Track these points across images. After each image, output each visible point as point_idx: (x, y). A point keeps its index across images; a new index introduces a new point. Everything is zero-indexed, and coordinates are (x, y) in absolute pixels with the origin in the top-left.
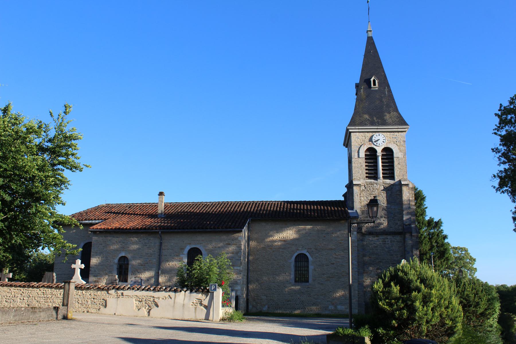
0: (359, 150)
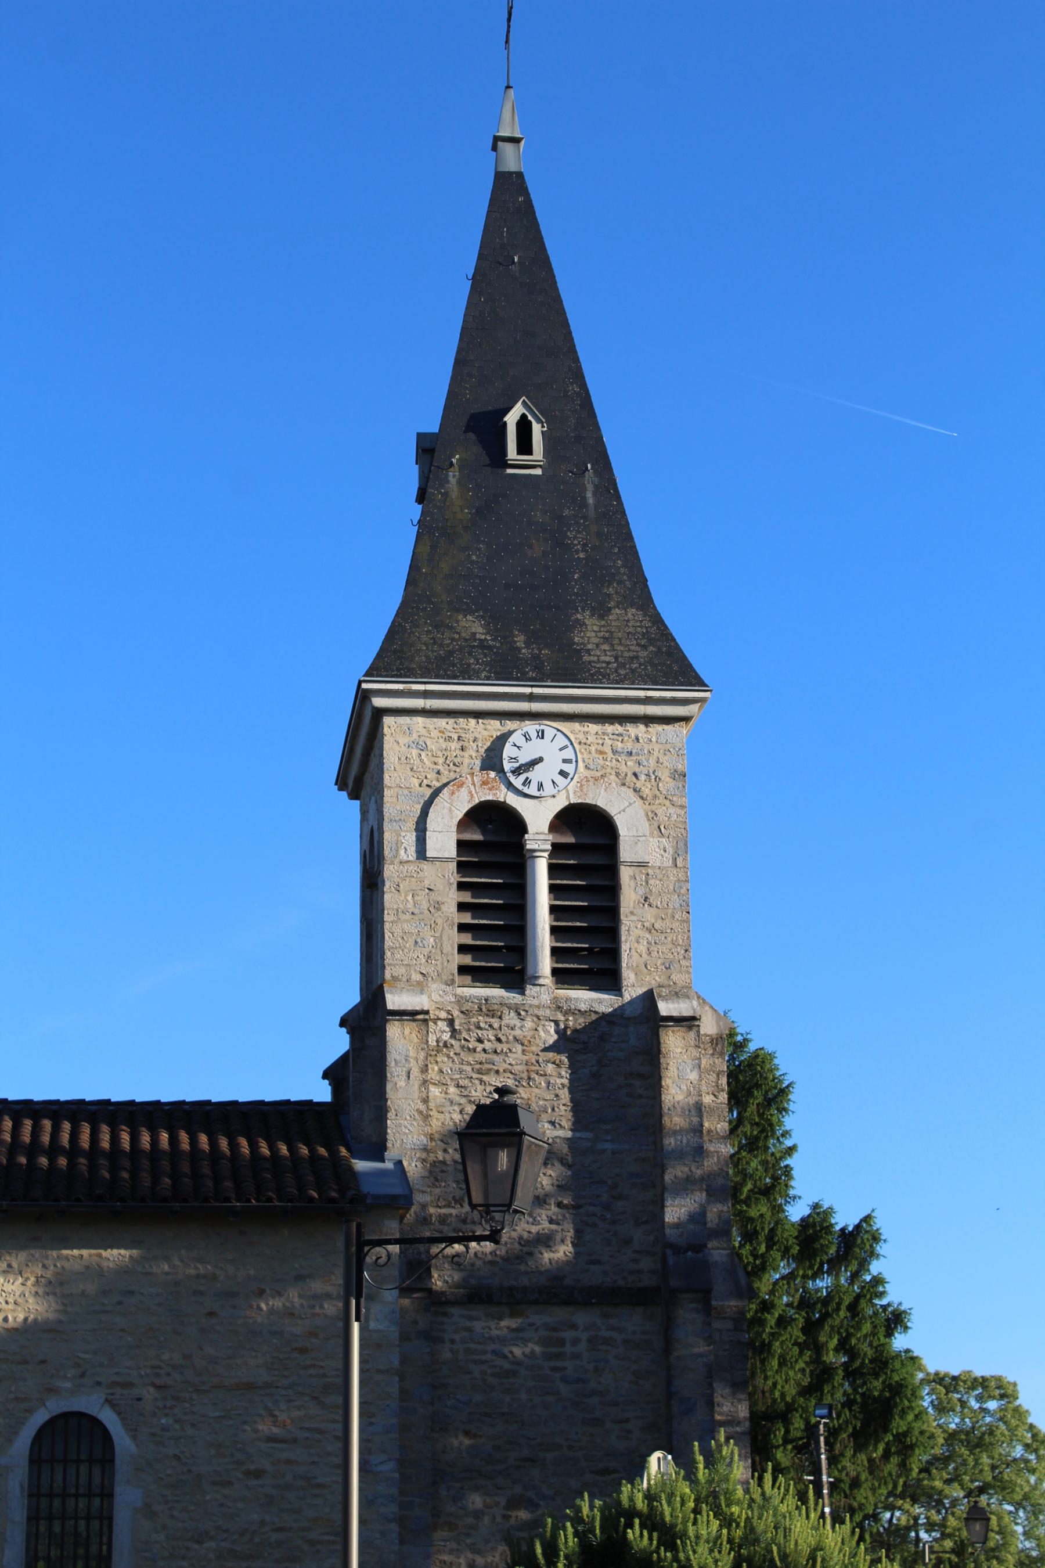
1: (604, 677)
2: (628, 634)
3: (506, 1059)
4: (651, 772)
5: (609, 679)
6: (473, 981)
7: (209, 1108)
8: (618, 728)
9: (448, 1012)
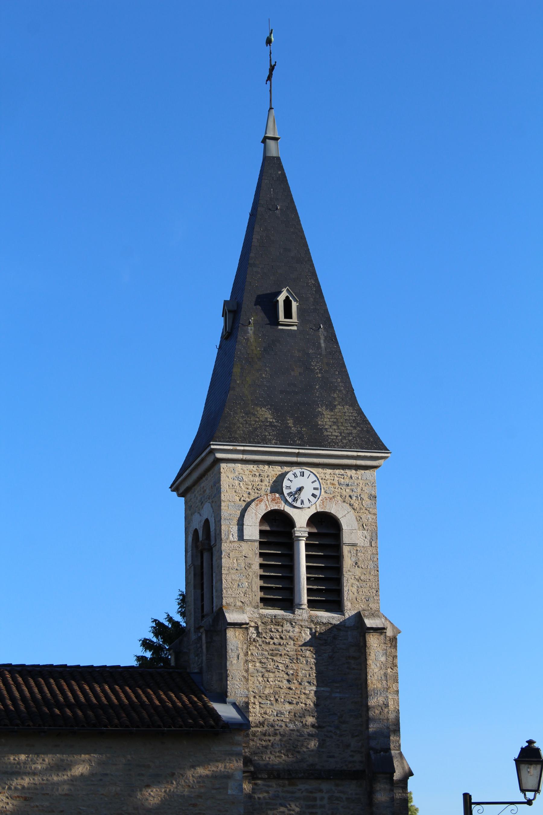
0: (483, 811)
1: (335, 444)
2: (346, 420)
3: (285, 648)
4: (358, 495)
5: (338, 445)
6: (264, 606)
7: (119, 670)
8: (342, 472)
9: (256, 623)
